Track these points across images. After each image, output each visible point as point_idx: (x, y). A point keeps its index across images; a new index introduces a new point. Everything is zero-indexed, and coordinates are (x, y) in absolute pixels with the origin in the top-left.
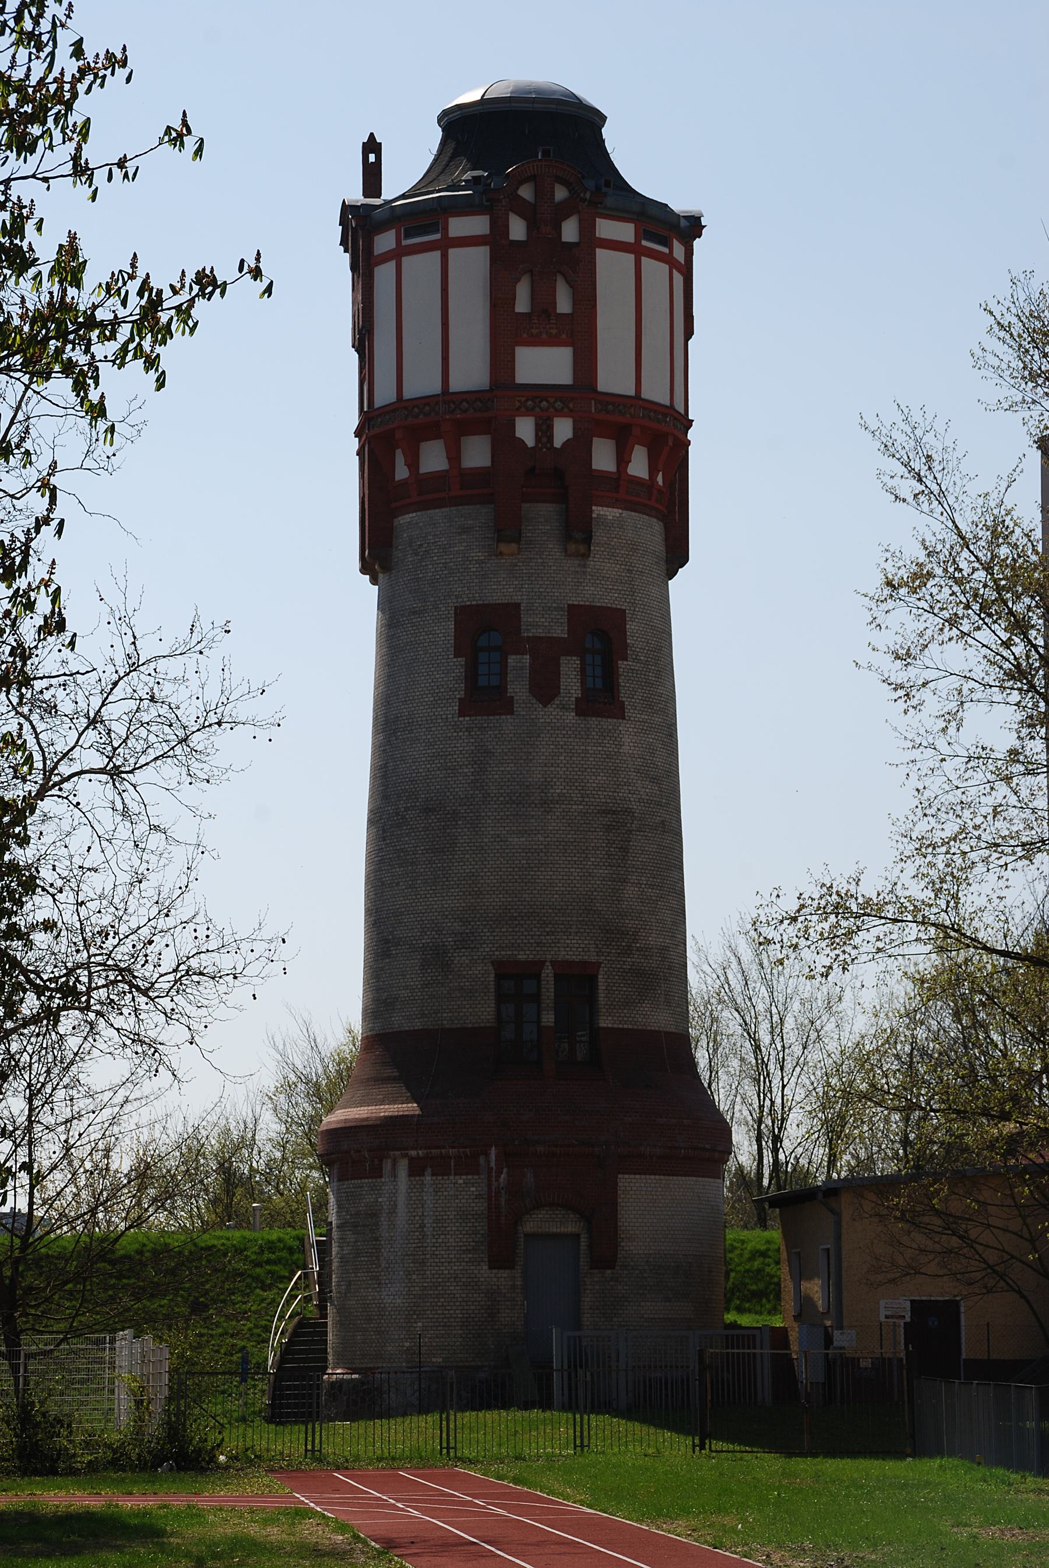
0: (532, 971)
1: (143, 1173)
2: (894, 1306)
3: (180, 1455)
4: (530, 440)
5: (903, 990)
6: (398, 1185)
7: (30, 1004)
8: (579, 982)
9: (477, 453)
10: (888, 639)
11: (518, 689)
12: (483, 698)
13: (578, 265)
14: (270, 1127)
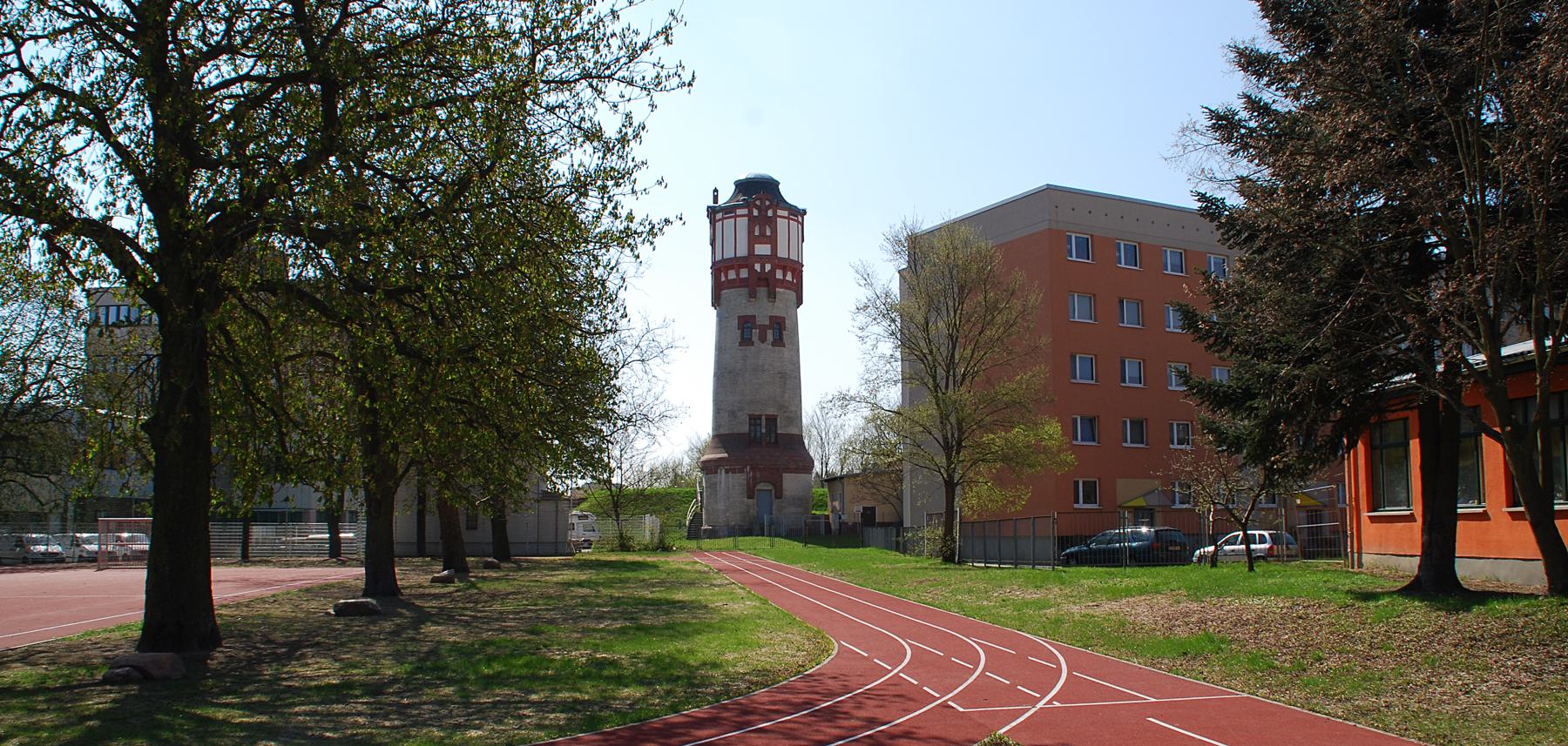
0: (759, 417)
1: (652, 472)
2: (858, 508)
3: (664, 548)
5: (861, 422)
6: (722, 476)
7: (620, 423)
8: (772, 420)
9: (744, 273)
10: (857, 324)
11: (755, 339)
12: (746, 341)
13: (772, 222)
14: (687, 461)
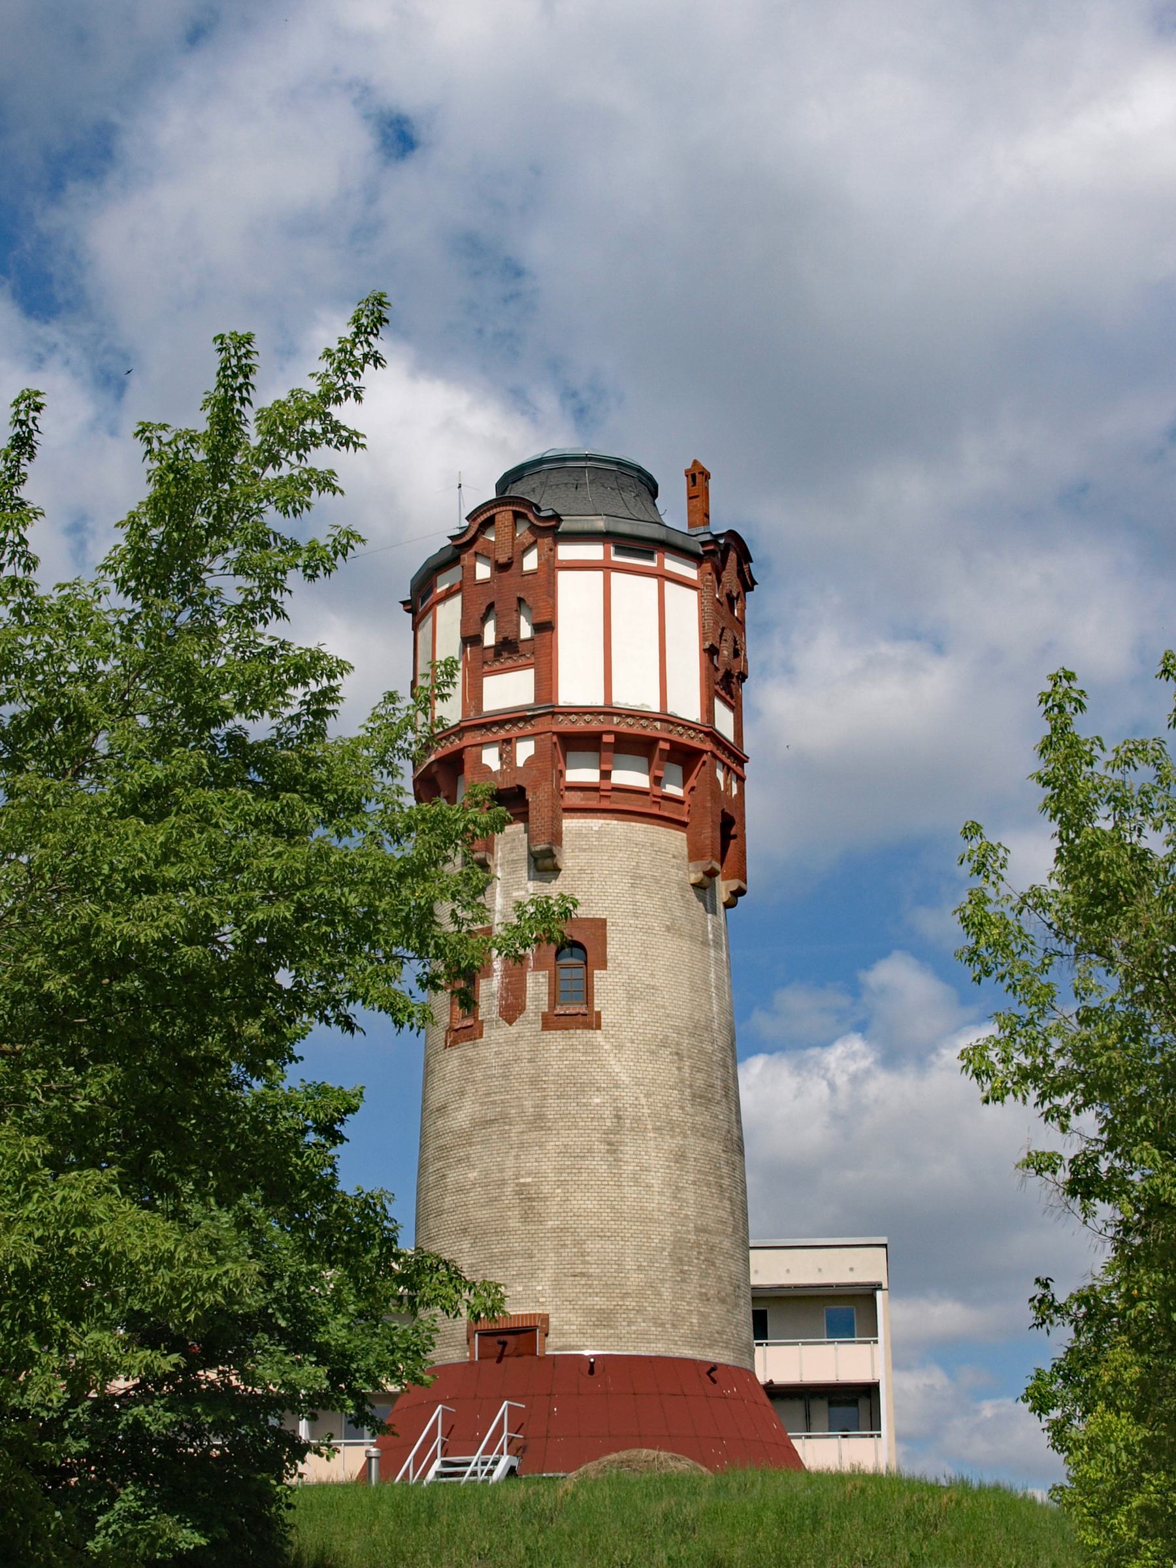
4: (495, 765)
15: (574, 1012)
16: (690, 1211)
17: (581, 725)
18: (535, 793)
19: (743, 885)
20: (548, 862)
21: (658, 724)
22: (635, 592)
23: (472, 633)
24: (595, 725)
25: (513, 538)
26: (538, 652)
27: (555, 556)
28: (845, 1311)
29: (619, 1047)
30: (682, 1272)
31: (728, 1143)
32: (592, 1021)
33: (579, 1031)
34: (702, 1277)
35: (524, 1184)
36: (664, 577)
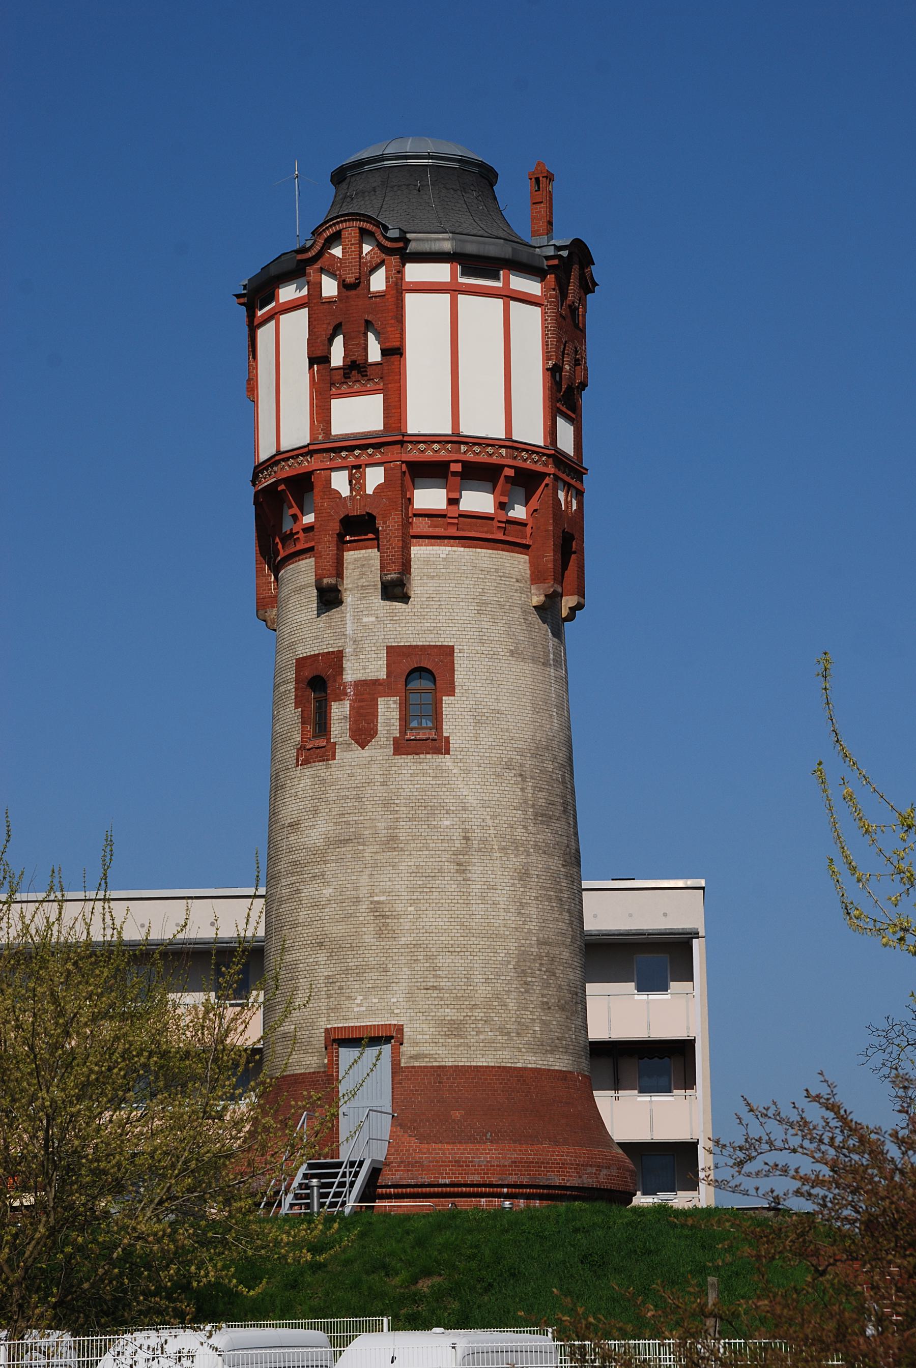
4: (345, 491)
15: (424, 737)
16: (532, 926)
17: (429, 454)
18: (385, 523)
19: (581, 600)
20: (397, 591)
21: (503, 451)
22: (481, 314)
23: (319, 353)
24: (443, 455)
25: (360, 258)
26: (386, 376)
27: (402, 278)
28: (657, 958)
29: (467, 771)
30: (525, 983)
31: (567, 857)
32: (440, 746)
33: (429, 756)
34: (543, 988)
35: (378, 902)
36: (510, 296)
